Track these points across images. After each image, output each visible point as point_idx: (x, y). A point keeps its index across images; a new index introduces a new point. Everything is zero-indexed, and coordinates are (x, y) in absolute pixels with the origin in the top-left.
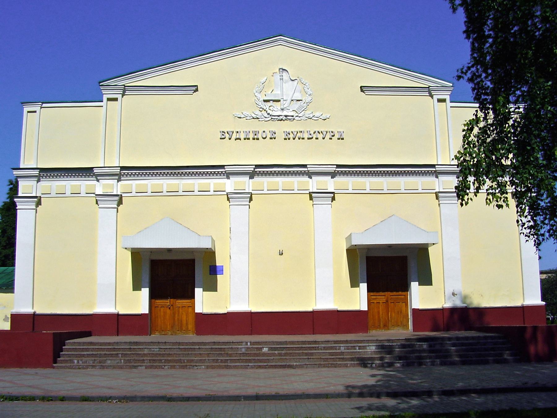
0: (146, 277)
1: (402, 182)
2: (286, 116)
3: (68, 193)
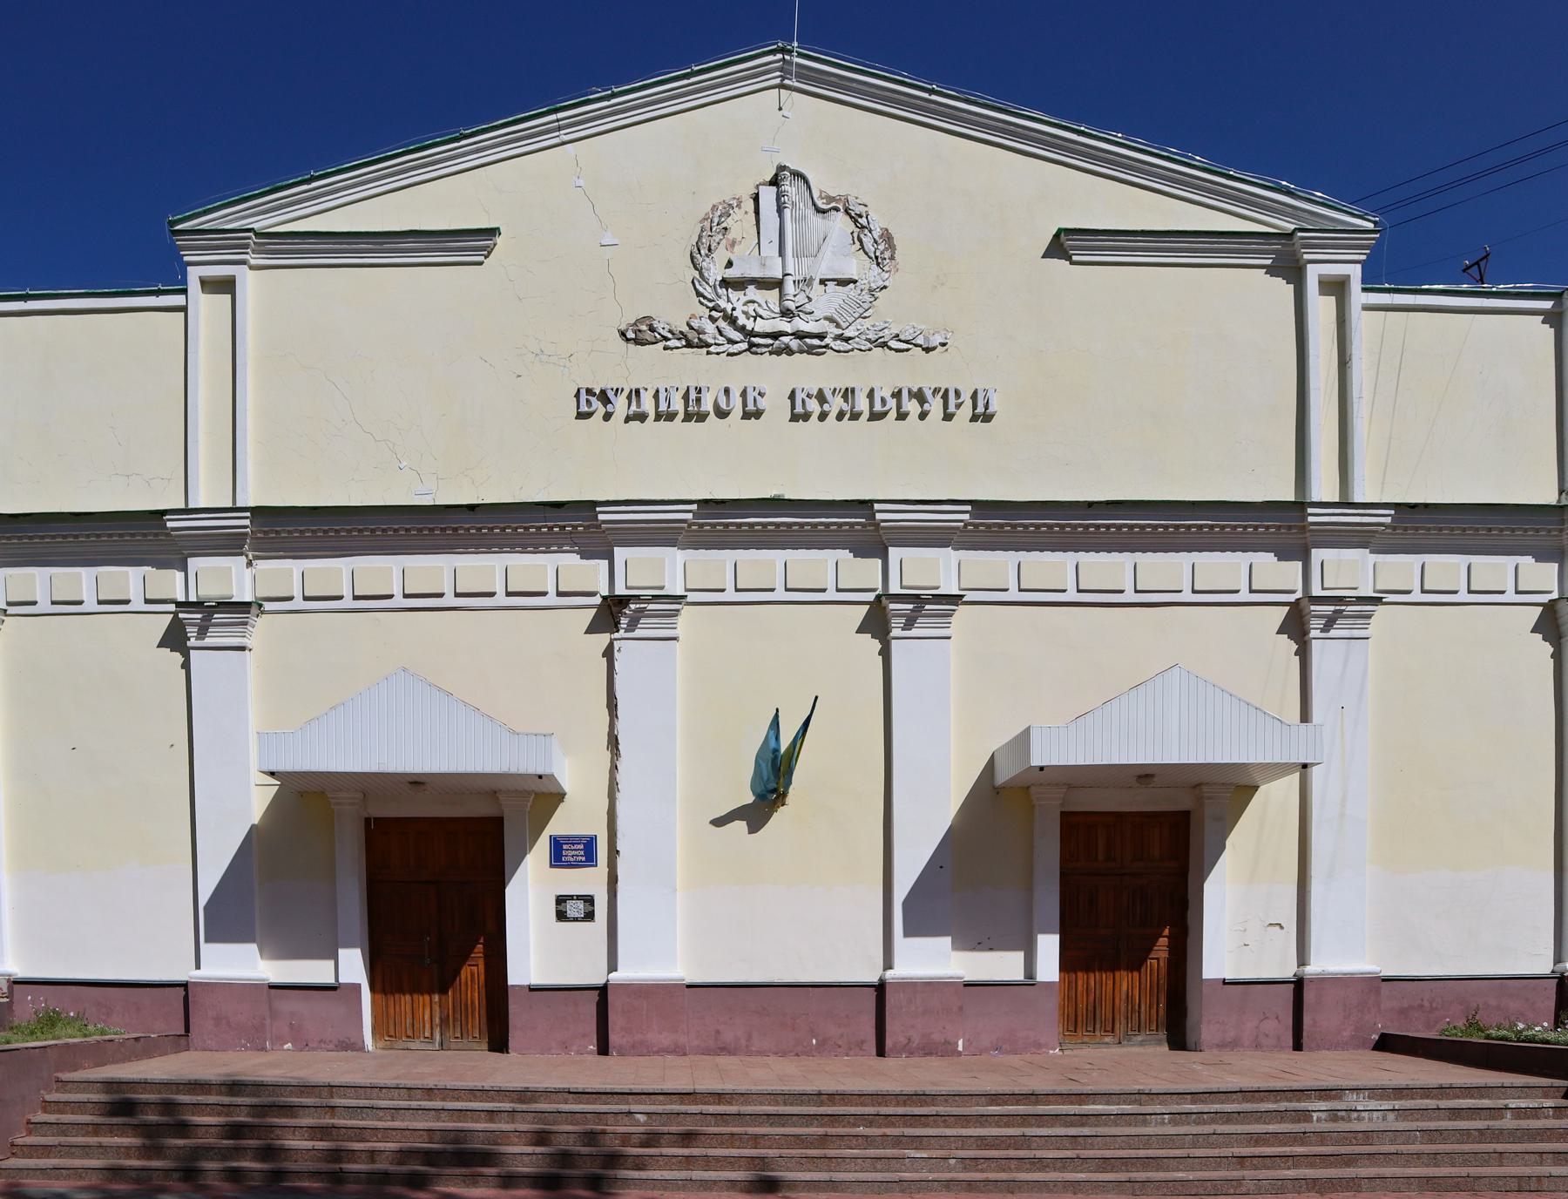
1: (1166, 569)
2: (800, 335)
3: (90, 605)
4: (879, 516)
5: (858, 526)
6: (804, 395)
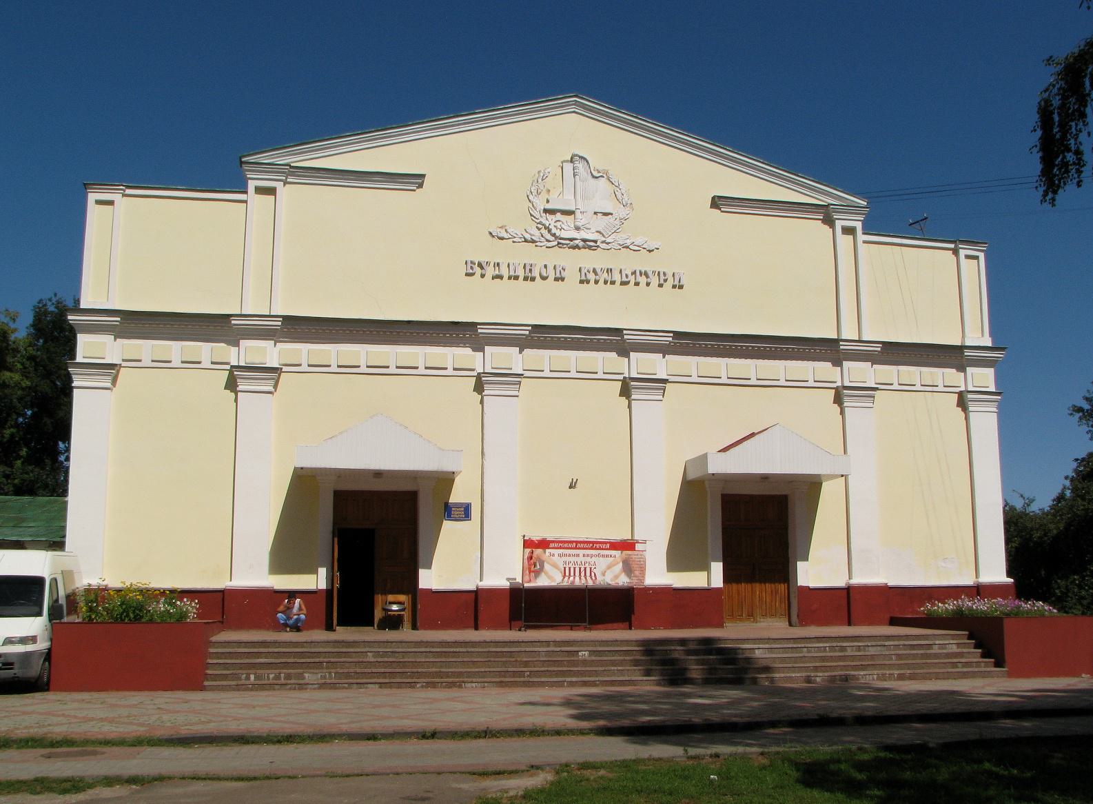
0: (714, 539)
2: (584, 241)
3: (176, 363)
4: (626, 337)
5: (614, 340)
6: (561, 268)
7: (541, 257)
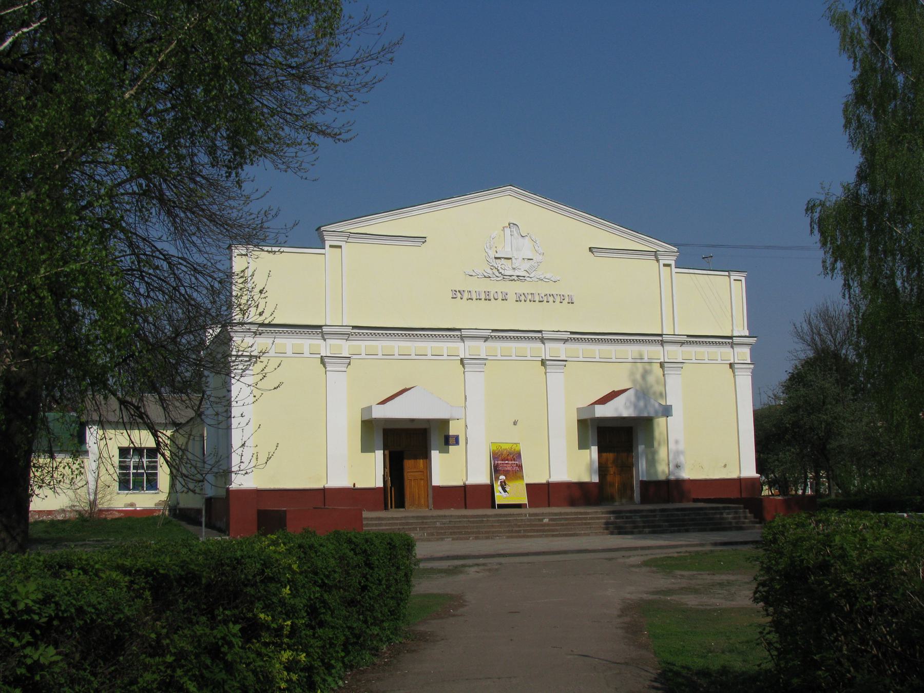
3: (289, 353)
5: (539, 336)
7: (497, 287)
